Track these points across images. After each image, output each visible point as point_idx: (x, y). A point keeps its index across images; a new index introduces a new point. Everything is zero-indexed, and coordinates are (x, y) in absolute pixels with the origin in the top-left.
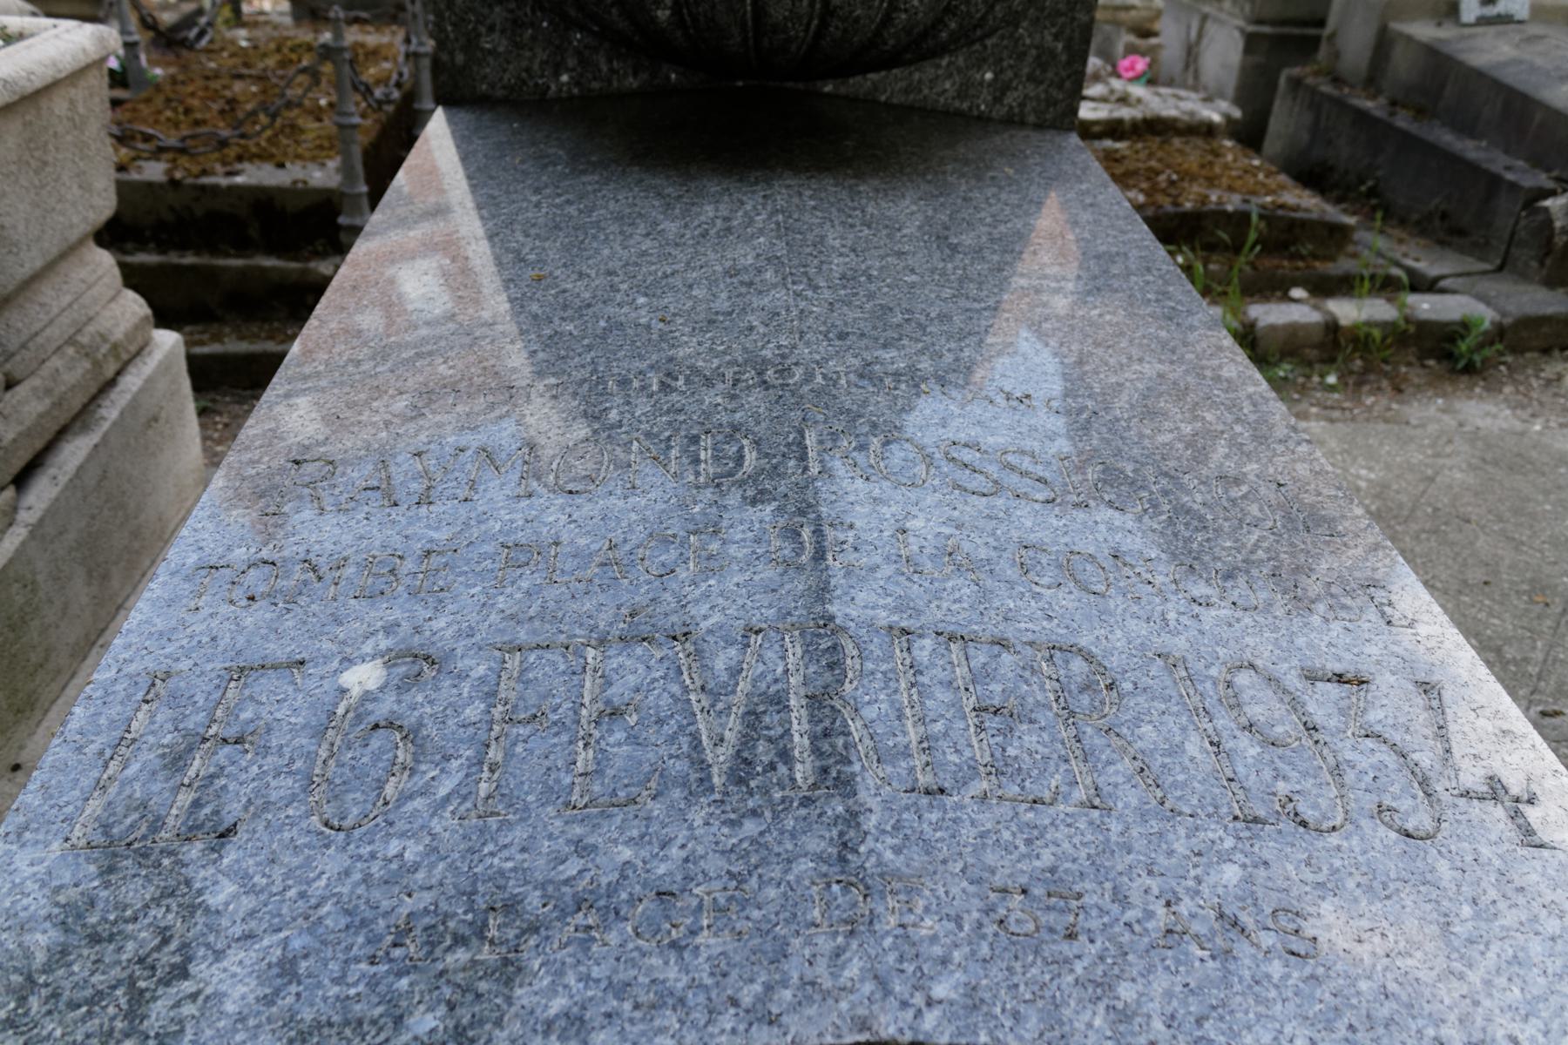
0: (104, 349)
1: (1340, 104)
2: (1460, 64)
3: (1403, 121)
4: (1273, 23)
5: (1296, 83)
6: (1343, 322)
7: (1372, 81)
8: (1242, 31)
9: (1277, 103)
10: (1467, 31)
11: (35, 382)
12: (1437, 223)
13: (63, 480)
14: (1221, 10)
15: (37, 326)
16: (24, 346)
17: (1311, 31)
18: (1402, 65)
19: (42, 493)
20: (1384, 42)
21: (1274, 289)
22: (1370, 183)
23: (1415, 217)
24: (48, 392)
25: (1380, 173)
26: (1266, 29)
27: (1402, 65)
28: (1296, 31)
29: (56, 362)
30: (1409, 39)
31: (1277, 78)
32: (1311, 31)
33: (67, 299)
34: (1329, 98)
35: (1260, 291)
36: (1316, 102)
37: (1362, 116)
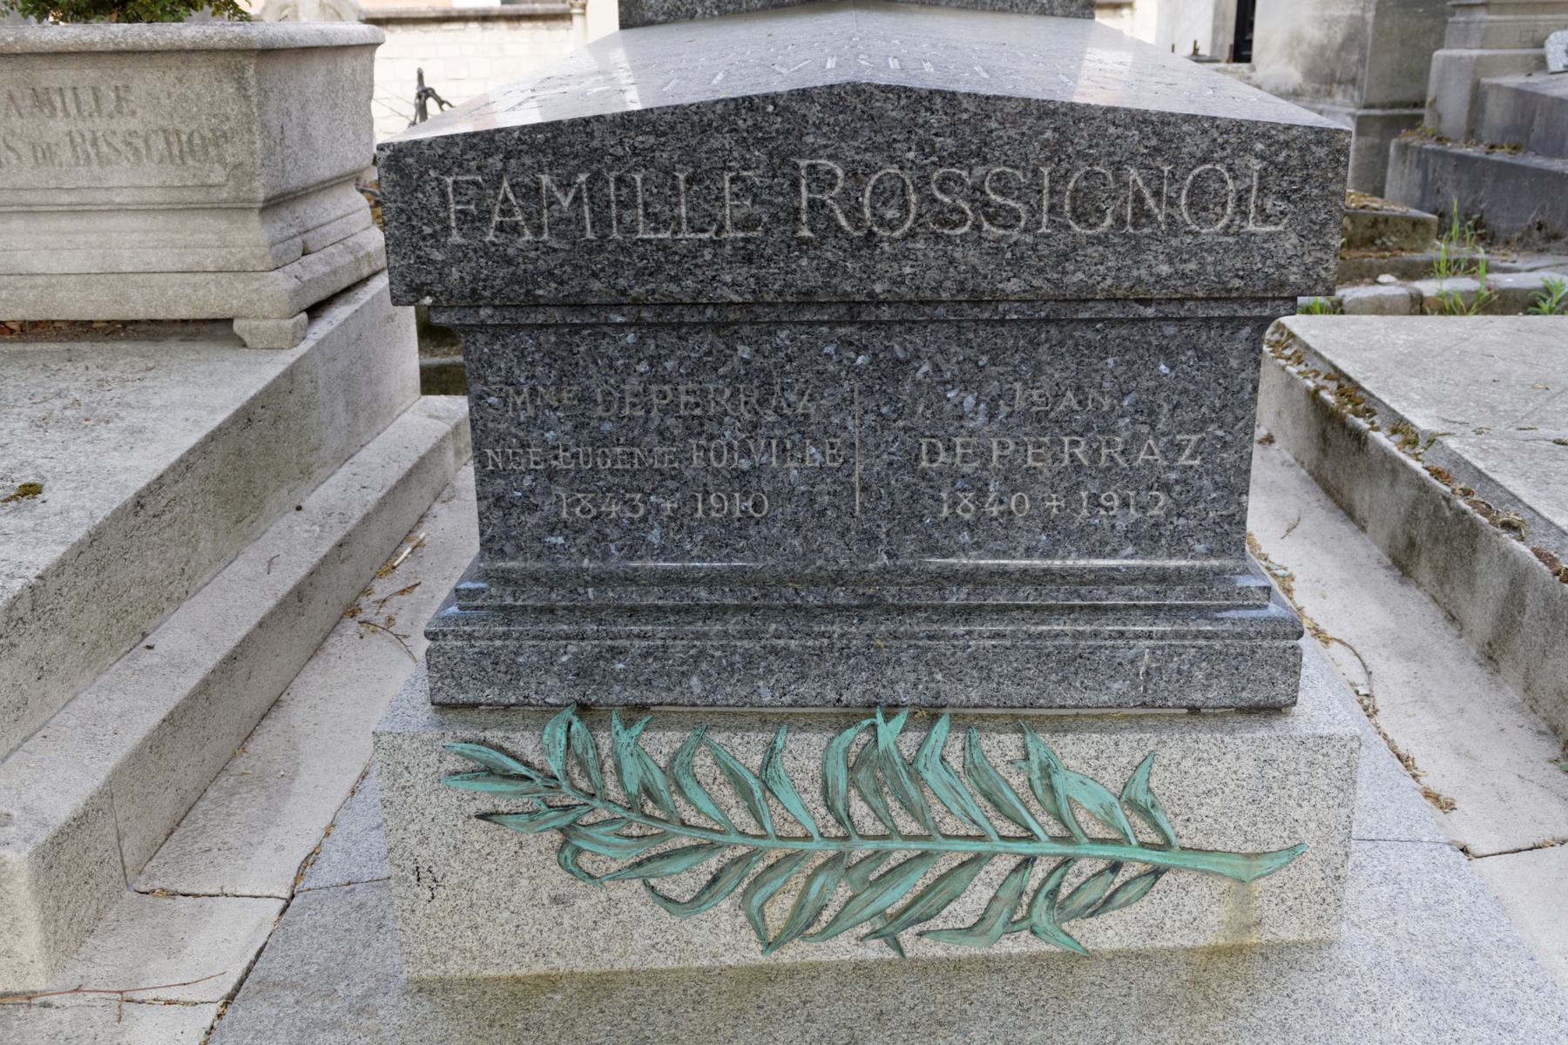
0: (362, 253)
1: (1443, 155)
2: (1544, 96)
3: (1499, 156)
4: (1383, 107)
5: (1404, 149)
6: (1427, 294)
7: (1472, 134)
8: (1352, 115)
9: (1390, 170)
10: (1554, 77)
11: (321, 255)
12: (1536, 234)
13: (336, 323)
14: (1334, 104)
15: (322, 221)
16: (315, 228)
17: (1416, 111)
18: (1497, 113)
19: (322, 328)
20: (1477, 98)
21: (1362, 277)
22: (1475, 216)
23: (1517, 235)
24: (328, 263)
25: (1482, 206)
26: (1378, 112)
27: (1497, 113)
28: (1407, 112)
29: (332, 249)
30: (1499, 87)
31: (1387, 150)
32: (1416, 111)
33: (340, 213)
34: (1434, 152)
35: (1350, 279)
36: (1423, 160)
37: (1462, 159)
